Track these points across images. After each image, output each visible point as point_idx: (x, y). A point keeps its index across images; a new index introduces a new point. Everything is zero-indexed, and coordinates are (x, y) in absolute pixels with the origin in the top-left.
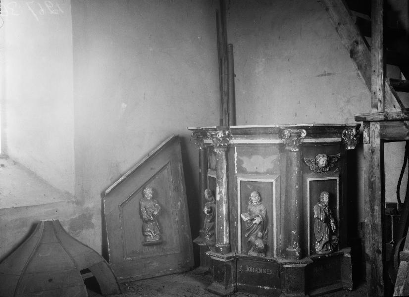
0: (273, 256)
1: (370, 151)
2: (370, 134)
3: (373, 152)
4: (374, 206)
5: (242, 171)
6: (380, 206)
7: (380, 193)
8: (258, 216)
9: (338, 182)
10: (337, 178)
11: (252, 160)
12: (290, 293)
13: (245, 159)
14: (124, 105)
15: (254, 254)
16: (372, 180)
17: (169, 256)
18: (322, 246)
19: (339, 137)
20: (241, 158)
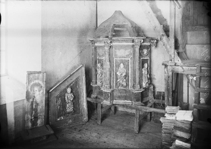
0: (129, 88)
1: (168, 77)
2: (167, 70)
3: (169, 77)
4: (169, 98)
5: (116, 55)
6: (172, 98)
7: (172, 93)
8: (124, 73)
9: (149, 60)
10: (149, 58)
11: (120, 51)
12: (136, 102)
13: (117, 51)
14: (61, 53)
15: (122, 88)
16: (168, 88)
17: (86, 129)
18: (145, 84)
19: (149, 43)
20: (116, 51)
